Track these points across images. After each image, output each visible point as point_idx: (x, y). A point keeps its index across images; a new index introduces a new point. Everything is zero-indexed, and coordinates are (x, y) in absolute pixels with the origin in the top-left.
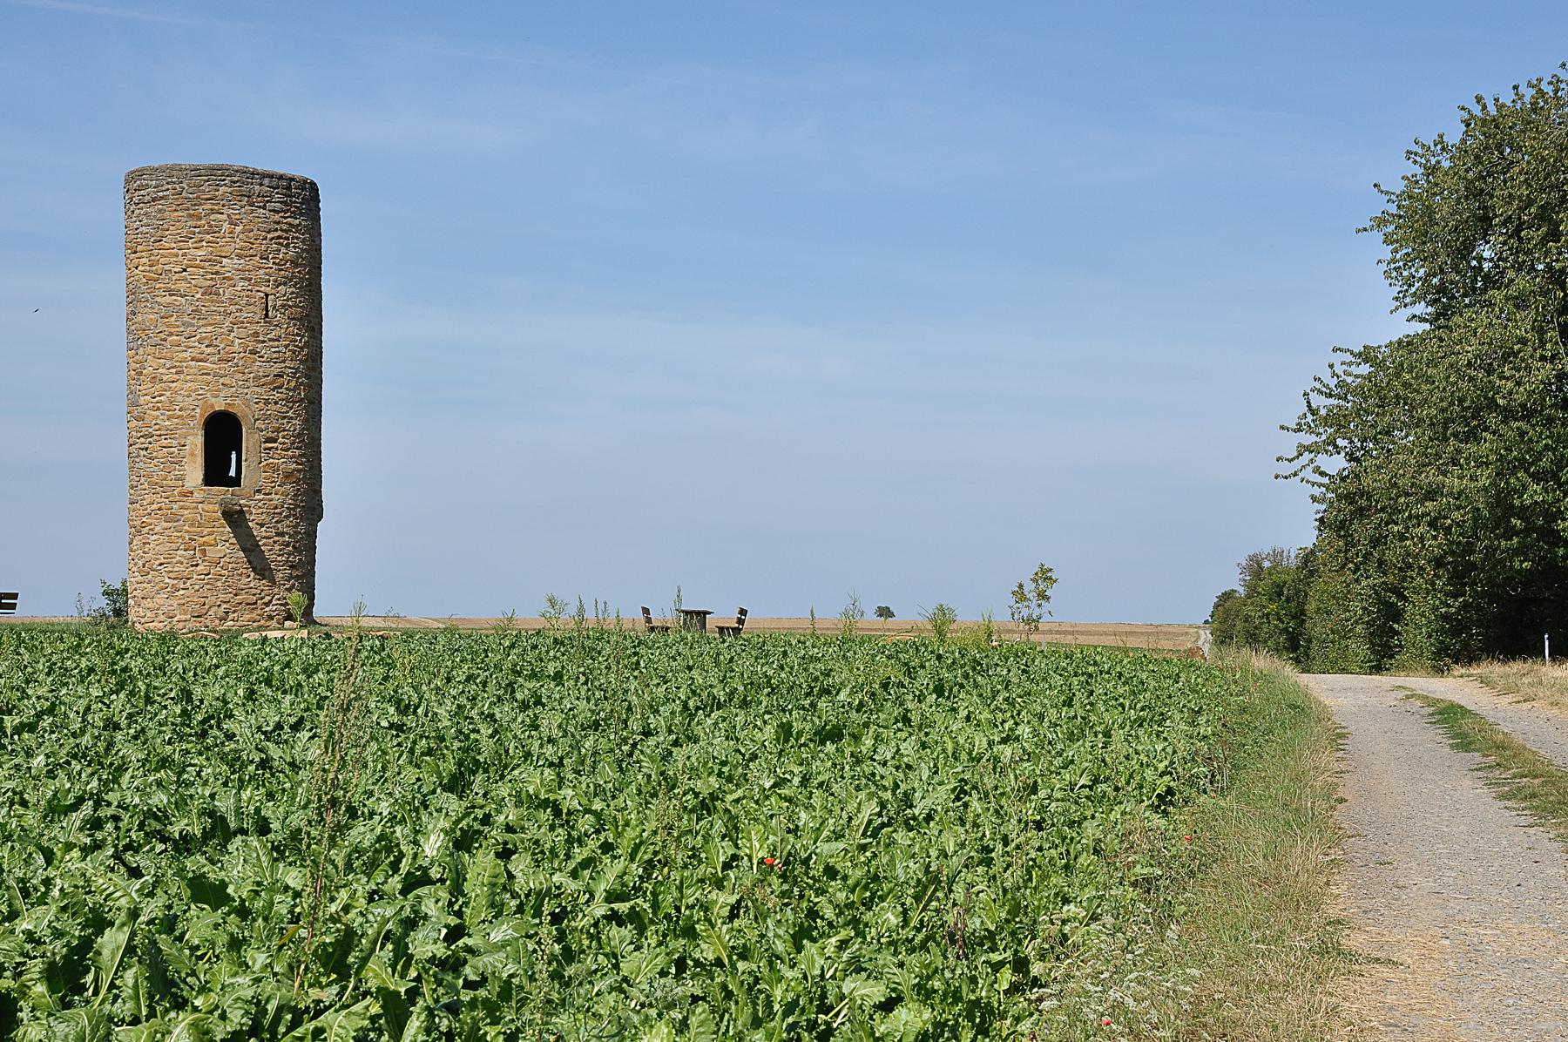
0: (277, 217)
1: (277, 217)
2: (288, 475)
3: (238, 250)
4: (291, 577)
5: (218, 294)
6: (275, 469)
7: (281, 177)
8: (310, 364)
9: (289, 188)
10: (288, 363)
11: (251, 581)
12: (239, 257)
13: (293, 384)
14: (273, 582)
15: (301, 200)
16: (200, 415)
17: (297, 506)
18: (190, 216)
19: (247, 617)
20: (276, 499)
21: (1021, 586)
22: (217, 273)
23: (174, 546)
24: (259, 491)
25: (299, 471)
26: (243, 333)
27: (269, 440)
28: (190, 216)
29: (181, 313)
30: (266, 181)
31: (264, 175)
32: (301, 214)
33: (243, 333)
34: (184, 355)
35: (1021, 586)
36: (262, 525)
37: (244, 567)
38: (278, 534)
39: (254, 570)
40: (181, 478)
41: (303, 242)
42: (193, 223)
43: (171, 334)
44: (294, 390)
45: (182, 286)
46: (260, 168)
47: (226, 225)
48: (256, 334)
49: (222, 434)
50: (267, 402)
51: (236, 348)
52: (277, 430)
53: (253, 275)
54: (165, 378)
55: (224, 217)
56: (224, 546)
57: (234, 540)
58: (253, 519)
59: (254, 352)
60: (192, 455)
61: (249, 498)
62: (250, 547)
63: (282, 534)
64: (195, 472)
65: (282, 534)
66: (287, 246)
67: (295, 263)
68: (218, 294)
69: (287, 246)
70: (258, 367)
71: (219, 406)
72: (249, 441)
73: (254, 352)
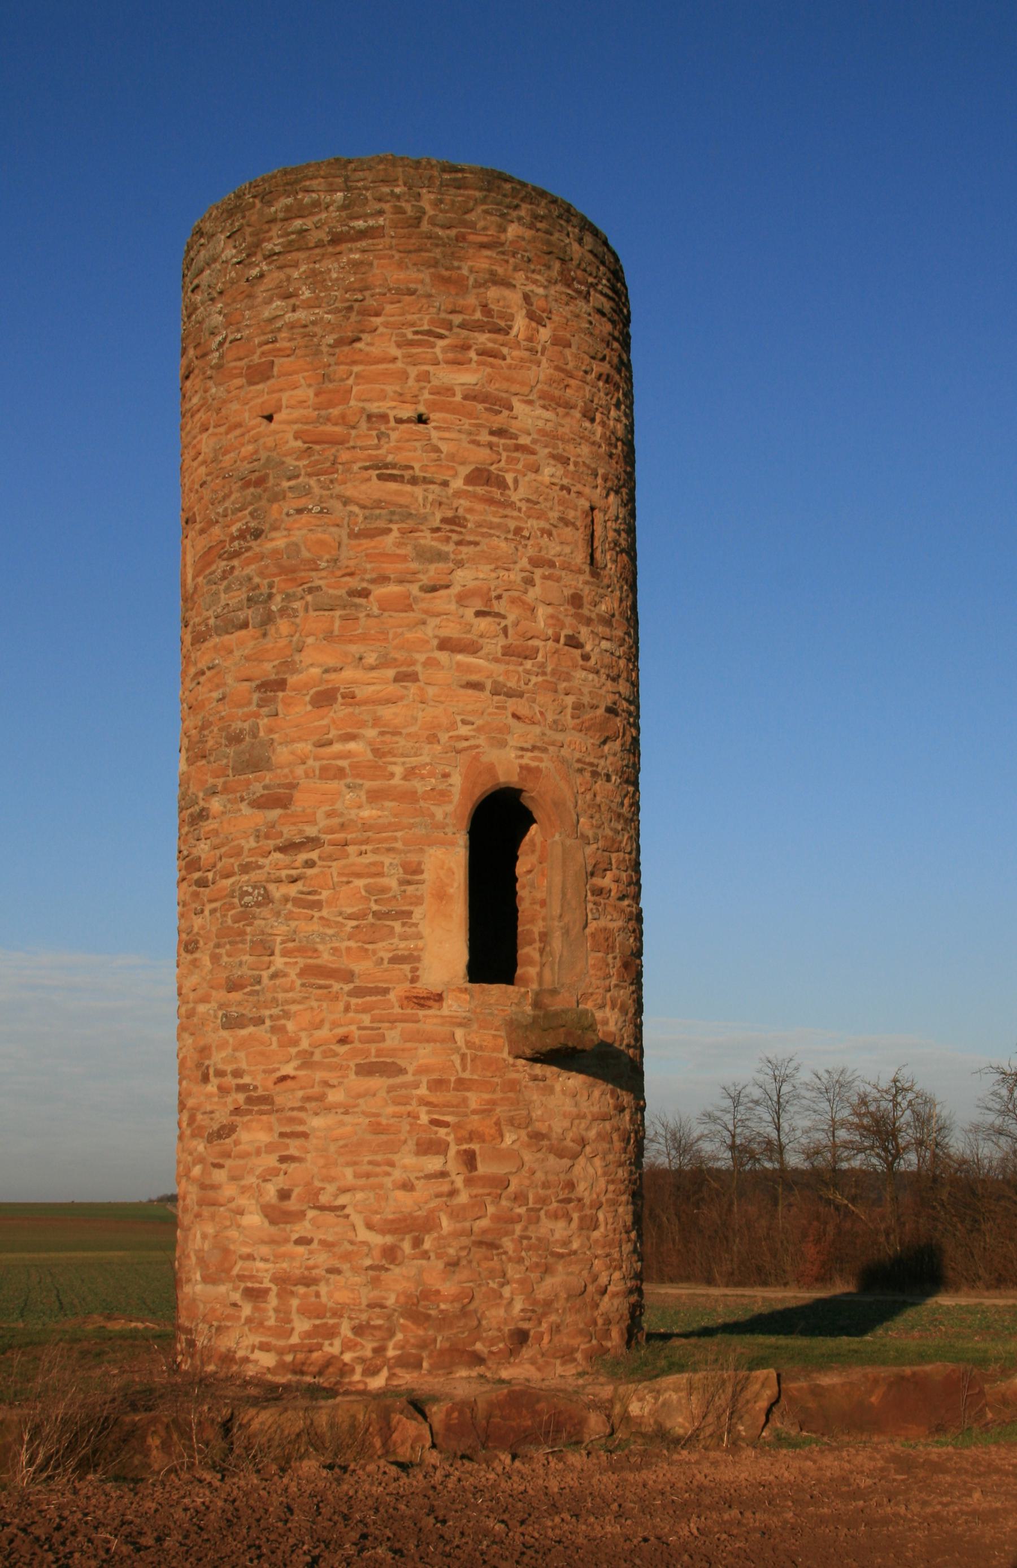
22: (500, 433)
40: (411, 959)
48: (576, 600)
60: (441, 895)
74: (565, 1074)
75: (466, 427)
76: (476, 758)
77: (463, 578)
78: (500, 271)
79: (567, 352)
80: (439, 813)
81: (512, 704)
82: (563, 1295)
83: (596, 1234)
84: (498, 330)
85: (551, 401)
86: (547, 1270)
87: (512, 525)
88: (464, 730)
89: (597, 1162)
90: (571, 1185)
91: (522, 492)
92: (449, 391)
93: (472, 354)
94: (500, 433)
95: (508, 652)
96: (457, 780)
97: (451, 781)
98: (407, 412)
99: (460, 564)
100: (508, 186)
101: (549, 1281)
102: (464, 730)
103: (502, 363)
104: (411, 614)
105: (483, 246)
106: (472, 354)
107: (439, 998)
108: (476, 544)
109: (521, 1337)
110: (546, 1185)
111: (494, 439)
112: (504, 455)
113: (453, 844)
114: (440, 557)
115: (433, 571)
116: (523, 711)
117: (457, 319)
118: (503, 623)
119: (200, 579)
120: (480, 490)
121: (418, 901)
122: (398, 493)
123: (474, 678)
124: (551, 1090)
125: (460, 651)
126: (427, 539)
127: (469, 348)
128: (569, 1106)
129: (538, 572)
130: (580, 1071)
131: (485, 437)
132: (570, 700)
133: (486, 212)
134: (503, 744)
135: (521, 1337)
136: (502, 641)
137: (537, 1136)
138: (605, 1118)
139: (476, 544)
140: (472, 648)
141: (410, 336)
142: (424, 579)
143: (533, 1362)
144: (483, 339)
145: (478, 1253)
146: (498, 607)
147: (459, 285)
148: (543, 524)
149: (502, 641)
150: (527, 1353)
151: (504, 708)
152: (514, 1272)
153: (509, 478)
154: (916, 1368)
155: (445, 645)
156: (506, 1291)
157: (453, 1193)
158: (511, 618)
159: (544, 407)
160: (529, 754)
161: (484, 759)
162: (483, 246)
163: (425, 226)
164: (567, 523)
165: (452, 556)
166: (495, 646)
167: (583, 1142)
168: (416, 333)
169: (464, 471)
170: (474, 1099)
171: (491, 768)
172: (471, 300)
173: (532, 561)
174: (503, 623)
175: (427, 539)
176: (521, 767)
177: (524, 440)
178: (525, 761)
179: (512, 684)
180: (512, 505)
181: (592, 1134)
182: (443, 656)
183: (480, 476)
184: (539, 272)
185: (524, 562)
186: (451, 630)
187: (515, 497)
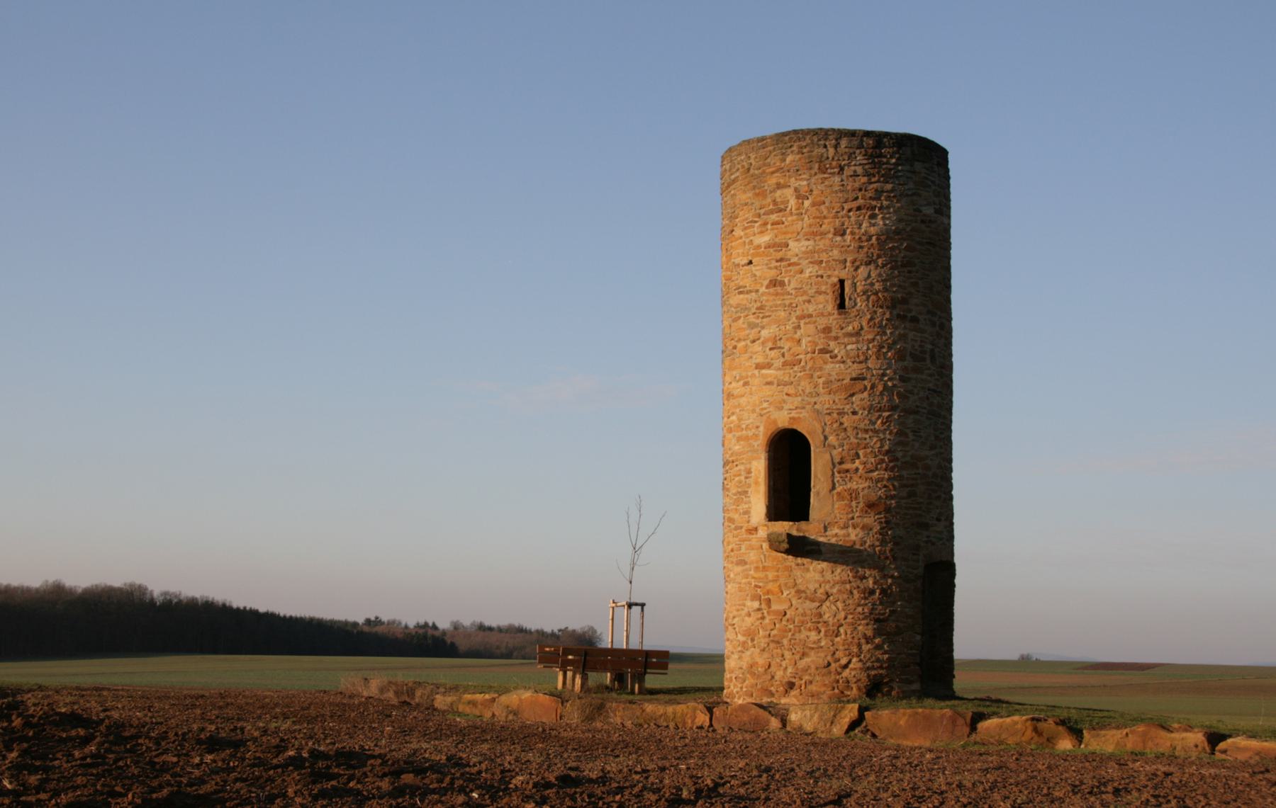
6: (853, 495)
8: (908, 362)
15: (904, 184)
16: (760, 444)
40: (747, 512)
43: (739, 340)
47: (793, 202)
48: (827, 330)
49: (789, 458)
53: (824, 257)
60: (757, 483)
64: (758, 504)
70: (833, 369)
71: (783, 420)
74: (815, 563)
77: (765, 333)
78: (782, 181)
79: (823, 207)
80: (756, 444)
81: (786, 389)
82: (813, 666)
83: (838, 639)
84: (781, 211)
85: (811, 235)
86: (804, 655)
87: (787, 302)
88: (765, 405)
89: (840, 605)
90: (820, 615)
91: (792, 285)
92: (759, 247)
93: (769, 226)
94: (781, 260)
95: (785, 364)
96: (762, 429)
98: (746, 261)
99: (763, 328)
100: (787, 138)
101: (807, 660)
102: (765, 405)
105: (773, 173)
106: (769, 226)
107: (756, 529)
109: (791, 685)
110: (804, 614)
114: (756, 325)
115: (753, 333)
116: (792, 391)
117: (762, 211)
120: (772, 290)
121: (749, 486)
123: (769, 379)
124: (808, 570)
126: (752, 319)
128: (817, 577)
129: (802, 322)
130: (824, 560)
131: (774, 264)
132: (821, 381)
134: (781, 409)
135: (791, 685)
136: (782, 360)
137: (799, 592)
138: (844, 583)
140: (769, 366)
142: (751, 337)
143: (795, 696)
144: (774, 217)
145: (772, 645)
146: (779, 344)
147: (762, 194)
148: (805, 298)
149: (782, 360)
150: (793, 693)
152: (787, 654)
153: (786, 280)
154: (900, 742)
155: (759, 367)
156: (784, 664)
157: (763, 618)
158: (786, 348)
162: (773, 173)
163: (752, 171)
164: (819, 293)
166: (778, 363)
167: (828, 595)
169: (766, 283)
170: (771, 575)
171: (775, 422)
172: (769, 200)
173: (797, 318)
175: (752, 319)
177: (794, 260)
179: (786, 379)
180: (789, 294)
181: (835, 591)
183: (773, 283)
185: (794, 319)
186: (760, 359)
187: (789, 289)
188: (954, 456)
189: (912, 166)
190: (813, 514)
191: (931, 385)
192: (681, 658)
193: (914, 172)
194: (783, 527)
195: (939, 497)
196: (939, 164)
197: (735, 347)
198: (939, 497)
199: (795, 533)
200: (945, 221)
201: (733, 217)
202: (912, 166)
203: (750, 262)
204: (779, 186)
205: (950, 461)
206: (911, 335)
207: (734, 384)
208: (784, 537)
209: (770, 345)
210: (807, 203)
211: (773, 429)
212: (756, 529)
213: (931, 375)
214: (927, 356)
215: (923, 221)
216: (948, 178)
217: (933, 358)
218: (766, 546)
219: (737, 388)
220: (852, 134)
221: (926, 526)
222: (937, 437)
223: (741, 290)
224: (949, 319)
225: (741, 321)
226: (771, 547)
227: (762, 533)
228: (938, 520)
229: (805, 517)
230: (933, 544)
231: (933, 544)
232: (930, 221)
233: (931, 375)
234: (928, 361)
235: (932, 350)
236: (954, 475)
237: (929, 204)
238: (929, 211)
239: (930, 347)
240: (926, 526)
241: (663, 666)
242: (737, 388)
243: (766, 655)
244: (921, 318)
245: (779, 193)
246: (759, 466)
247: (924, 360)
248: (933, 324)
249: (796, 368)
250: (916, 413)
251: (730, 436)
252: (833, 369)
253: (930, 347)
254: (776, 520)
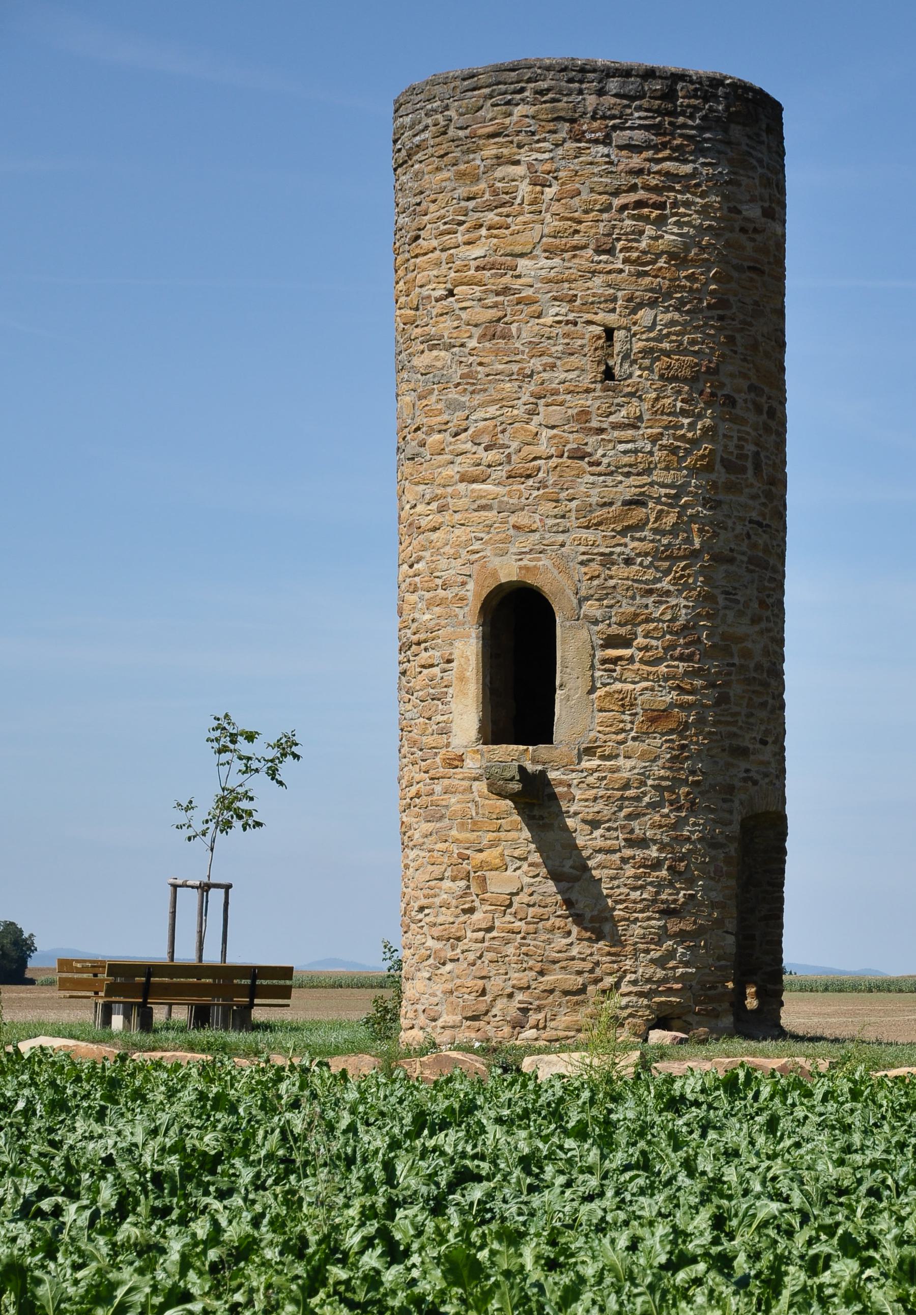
0: (636, 161)
1: (636, 161)
2: (656, 717)
3: (559, 243)
4: (663, 935)
5: (506, 336)
6: (626, 703)
7: (650, 74)
8: (720, 475)
9: (669, 95)
10: (658, 475)
11: (573, 944)
12: (550, 252)
13: (670, 520)
14: (617, 941)
15: (731, 134)
16: (474, 594)
17: (677, 782)
18: (461, 176)
19: (564, 1020)
20: (627, 767)
21: (252, 799)
22: (506, 291)
23: (437, 871)
24: (589, 751)
25: (682, 706)
26: (556, 414)
27: (611, 642)
28: (461, 176)
29: (444, 383)
30: (613, 85)
31: (609, 73)
32: (701, 151)
33: (556, 414)
34: (451, 471)
35: (252, 799)
36: (594, 824)
37: (557, 915)
38: (631, 843)
39: (578, 919)
40: (445, 732)
41: (704, 211)
42: (462, 191)
43: (431, 431)
44: (674, 531)
45: (446, 326)
46: (602, 59)
47: (524, 189)
48: (584, 415)
49: (518, 629)
50: (607, 560)
51: (543, 448)
52: (633, 620)
53: (579, 288)
54: (424, 522)
55: (520, 170)
56: (515, 866)
57: (536, 858)
58: (578, 806)
59: (579, 455)
60: (462, 679)
61: (566, 767)
62: (569, 872)
63: (643, 843)
64: (465, 714)
65: (643, 843)
66: (660, 222)
67: (677, 258)
68: (506, 336)
69: (660, 222)
70: (588, 487)
71: (508, 571)
72: (572, 648)
73: (579, 455)
75: (478, 294)
76: (484, 567)
97: (468, 587)
102: (477, 546)
103: (507, 232)
104: (445, 456)
107: (461, 758)
108: (485, 390)
111: (500, 299)
112: (509, 309)
113: (469, 637)
118: (507, 451)
119: (546, 433)
122: (437, 358)
123: (483, 502)
125: (474, 482)
126: (453, 394)
127: (481, 226)
133: (493, 105)
139: (485, 390)
141: (443, 227)
144: (491, 217)
151: (507, 522)
159: (547, 258)
160: (528, 556)
161: (490, 566)
163: (452, 132)
165: (467, 404)
168: (445, 223)
174: (507, 451)
175: (453, 394)
176: (520, 568)
178: (525, 562)
182: (462, 487)
184: (544, 140)
188: (787, 635)
189: (726, 131)
190: (560, 731)
191: (754, 515)
192: (314, 984)
193: (729, 143)
194: (511, 755)
195: (764, 705)
196: (769, 130)
197: (423, 444)
198: (764, 705)
199: (530, 767)
200: (779, 231)
201: (416, 211)
202: (726, 131)
203: (451, 293)
204: (500, 161)
205: (781, 642)
206: (724, 427)
207: (420, 508)
208: (514, 772)
209: (486, 440)
210: (549, 192)
211: (491, 585)
212: (461, 758)
213: (754, 497)
214: (749, 465)
215: (743, 230)
216: (781, 153)
217: (757, 467)
218: (481, 787)
219: (426, 515)
220: (626, 73)
221: (743, 752)
222: (762, 603)
223: (433, 343)
224: (783, 401)
225: (433, 398)
226: (491, 788)
227: (472, 764)
228: (764, 742)
229: (547, 738)
230: (755, 783)
231: (755, 783)
232: (755, 230)
233: (754, 497)
234: (750, 472)
235: (757, 454)
236: (786, 666)
237: (753, 200)
238: (753, 211)
239: (753, 448)
240: (743, 752)
241: (285, 993)
242: (426, 515)
243: (659, 1078)
244: (739, 398)
245: (500, 172)
246: (468, 649)
247: (743, 470)
248: (758, 409)
249: (530, 482)
250: (731, 561)
251: (413, 598)
252: (588, 487)
253: (753, 448)
254: (496, 741)
